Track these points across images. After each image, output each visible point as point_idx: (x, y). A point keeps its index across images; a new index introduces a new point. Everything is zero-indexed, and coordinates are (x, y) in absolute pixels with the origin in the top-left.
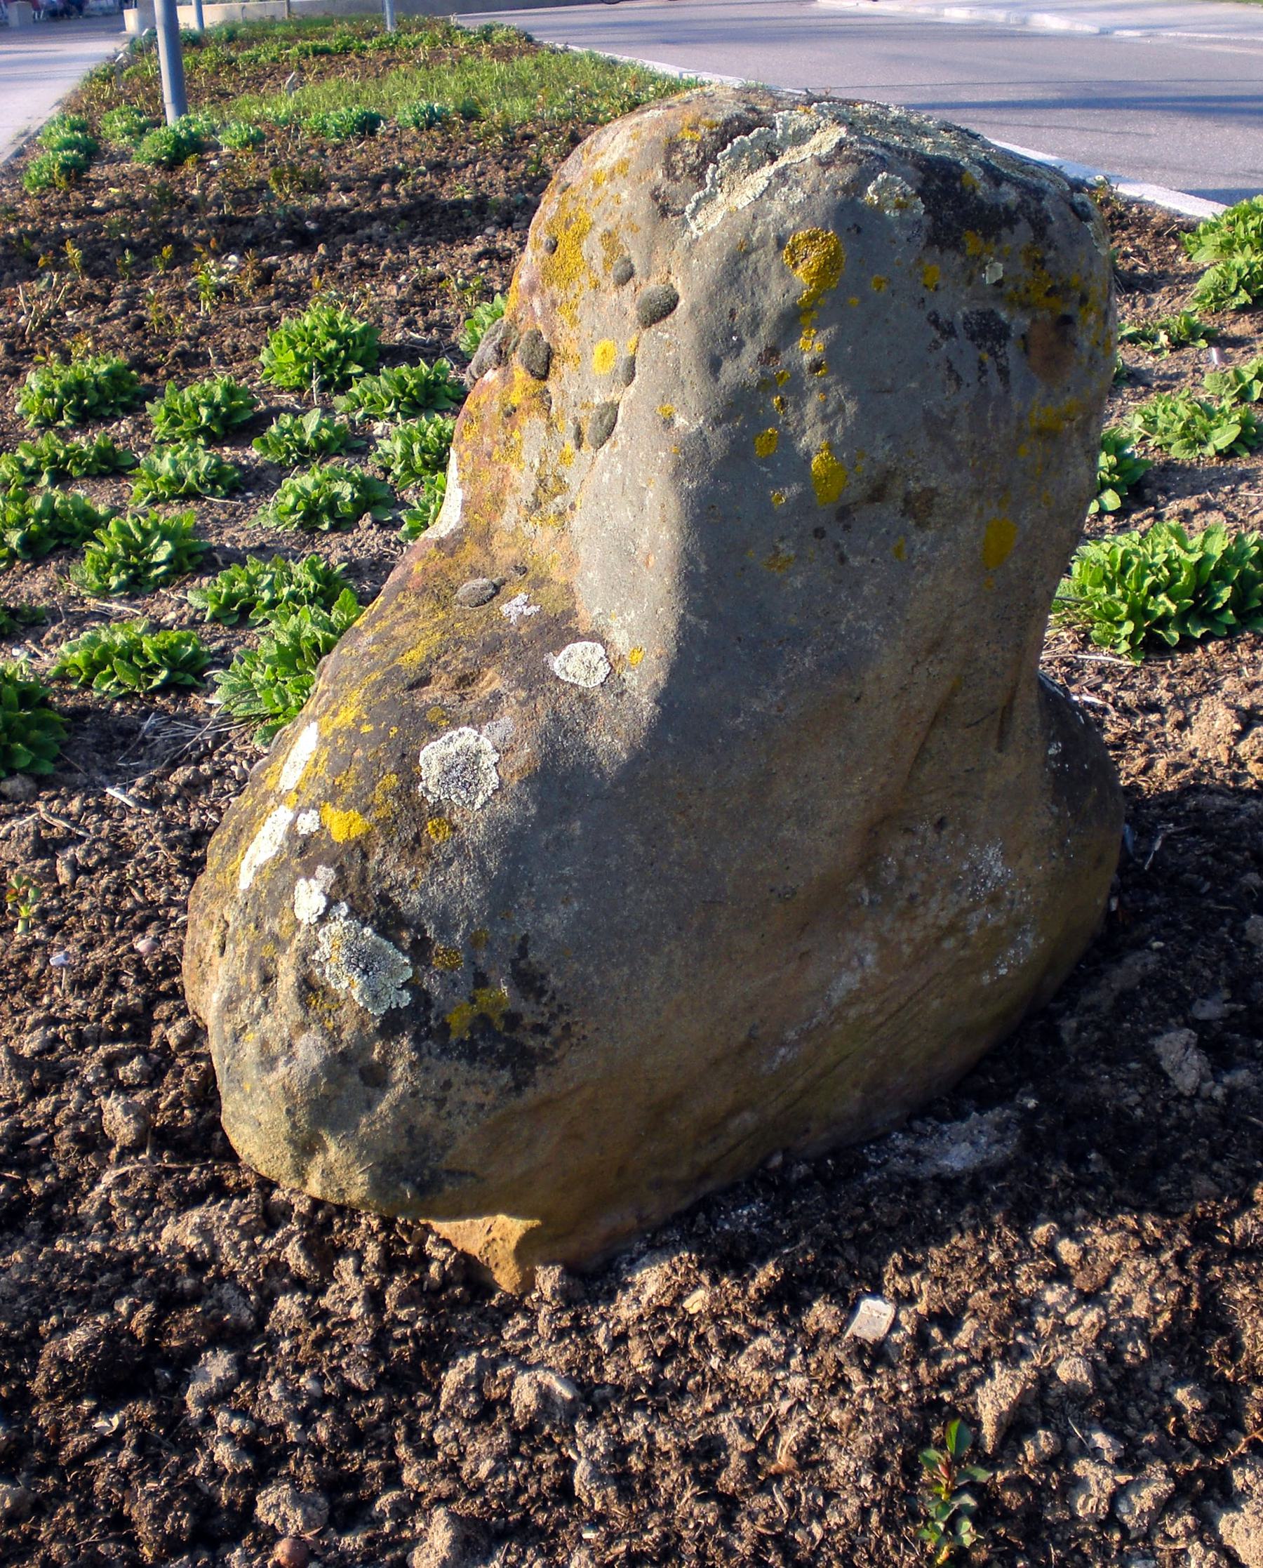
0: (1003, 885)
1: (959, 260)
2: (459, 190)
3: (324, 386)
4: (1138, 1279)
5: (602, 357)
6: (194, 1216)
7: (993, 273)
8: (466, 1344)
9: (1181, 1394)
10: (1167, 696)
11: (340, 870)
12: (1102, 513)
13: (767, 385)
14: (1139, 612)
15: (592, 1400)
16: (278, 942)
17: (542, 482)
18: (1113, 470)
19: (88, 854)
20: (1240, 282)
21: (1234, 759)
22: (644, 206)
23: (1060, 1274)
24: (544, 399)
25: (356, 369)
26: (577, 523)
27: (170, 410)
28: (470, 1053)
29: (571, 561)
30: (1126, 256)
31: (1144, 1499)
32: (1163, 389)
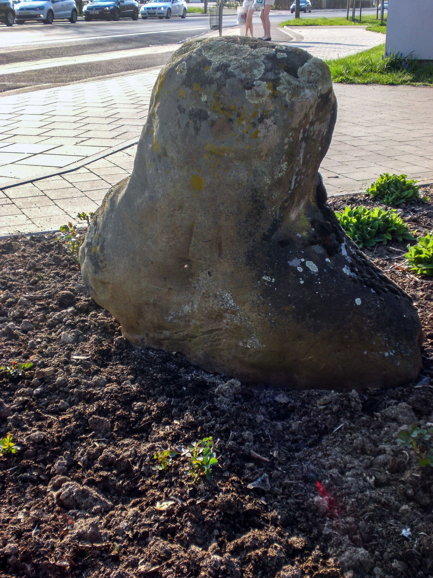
1: (190, 91)
7: (204, 98)
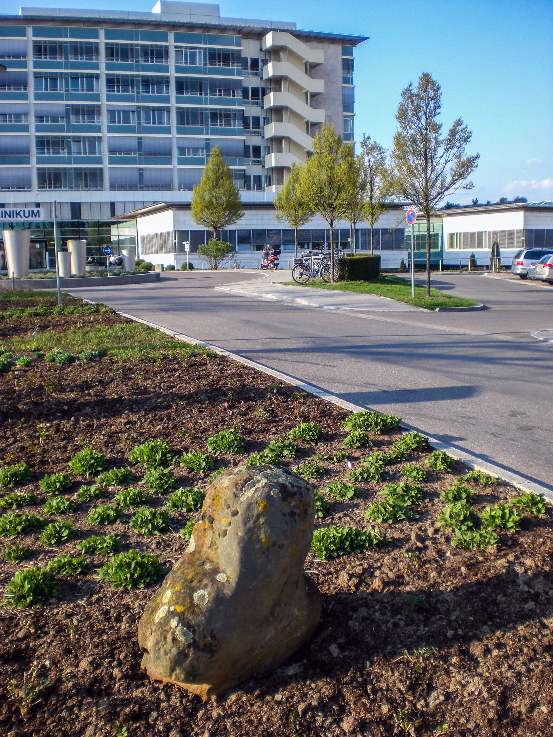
0: (298, 616)
2: (111, 394)
3: (90, 474)
4: (326, 689)
5: (224, 521)
6: (140, 690)
7: (293, 503)
8: (200, 709)
9: (334, 707)
10: (333, 570)
11: (180, 618)
12: (318, 518)
13: (255, 527)
14: (327, 549)
15: (227, 716)
16: (167, 631)
17: (212, 543)
18: (321, 506)
19: (81, 617)
20: (357, 440)
21: (348, 586)
22: (232, 496)
23: (312, 689)
24: (212, 528)
25: (100, 469)
26: (219, 551)
27: (47, 484)
28: (203, 650)
29: (218, 558)
30: (325, 427)
31: (328, 722)
32: (335, 476)
